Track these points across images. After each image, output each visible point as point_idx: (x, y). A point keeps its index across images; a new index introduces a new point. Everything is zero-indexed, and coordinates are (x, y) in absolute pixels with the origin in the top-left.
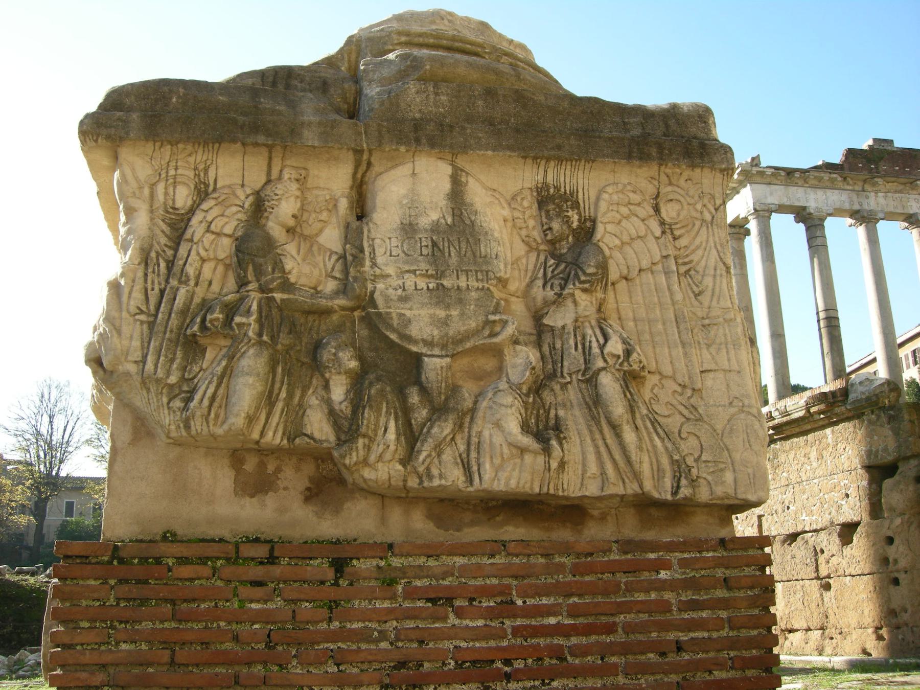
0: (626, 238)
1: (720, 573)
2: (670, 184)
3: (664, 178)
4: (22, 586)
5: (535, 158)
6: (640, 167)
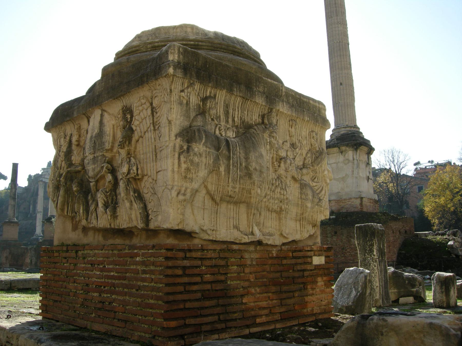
0: (140, 120)
1: (152, 259)
2: (155, 90)
3: (152, 88)
4: (433, 241)
5: (117, 98)
6: (143, 87)
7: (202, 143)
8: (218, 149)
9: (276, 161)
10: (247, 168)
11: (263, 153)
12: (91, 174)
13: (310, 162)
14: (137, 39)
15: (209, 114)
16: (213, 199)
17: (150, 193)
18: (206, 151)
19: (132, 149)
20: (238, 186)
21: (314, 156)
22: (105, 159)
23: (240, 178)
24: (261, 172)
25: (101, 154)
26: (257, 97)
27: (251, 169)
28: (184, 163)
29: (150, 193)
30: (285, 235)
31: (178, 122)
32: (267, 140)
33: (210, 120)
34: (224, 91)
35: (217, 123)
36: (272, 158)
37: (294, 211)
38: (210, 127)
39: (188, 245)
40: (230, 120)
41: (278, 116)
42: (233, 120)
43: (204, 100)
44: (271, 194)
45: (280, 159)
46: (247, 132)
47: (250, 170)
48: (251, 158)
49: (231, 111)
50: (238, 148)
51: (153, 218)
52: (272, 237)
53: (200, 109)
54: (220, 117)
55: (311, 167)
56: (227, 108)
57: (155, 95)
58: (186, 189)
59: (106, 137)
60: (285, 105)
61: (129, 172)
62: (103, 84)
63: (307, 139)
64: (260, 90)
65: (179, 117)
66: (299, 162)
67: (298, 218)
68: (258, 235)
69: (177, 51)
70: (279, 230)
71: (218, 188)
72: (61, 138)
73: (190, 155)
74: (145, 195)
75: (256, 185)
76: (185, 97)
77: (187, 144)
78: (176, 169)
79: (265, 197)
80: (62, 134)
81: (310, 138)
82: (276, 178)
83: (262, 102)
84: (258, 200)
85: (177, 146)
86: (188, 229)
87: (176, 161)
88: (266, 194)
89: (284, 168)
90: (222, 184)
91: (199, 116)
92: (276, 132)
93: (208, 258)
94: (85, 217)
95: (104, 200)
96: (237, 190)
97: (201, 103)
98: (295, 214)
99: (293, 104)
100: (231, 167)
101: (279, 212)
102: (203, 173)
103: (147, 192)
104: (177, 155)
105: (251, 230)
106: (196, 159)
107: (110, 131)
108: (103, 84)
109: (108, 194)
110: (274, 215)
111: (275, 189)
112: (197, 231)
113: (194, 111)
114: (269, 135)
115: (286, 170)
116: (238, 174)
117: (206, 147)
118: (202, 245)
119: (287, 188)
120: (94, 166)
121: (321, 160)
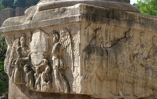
2: (72, 26)
7: (95, 54)
8: (102, 55)
9: (132, 57)
11: (125, 54)
13: (152, 54)
15: (98, 37)
16: (100, 79)
17: (70, 76)
18: (97, 57)
19: (60, 54)
20: (112, 72)
21: (155, 50)
24: (123, 64)
27: (118, 63)
28: (87, 64)
29: (70, 76)
30: (136, 95)
31: (84, 44)
32: (127, 46)
33: (98, 40)
34: (105, 24)
35: (102, 41)
36: (130, 55)
37: (141, 82)
38: (98, 45)
40: (108, 38)
41: (134, 32)
42: (110, 38)
43: (96, 31)
44: (129, 74)
45: (135, 56)
46: (116, 43)
47: (117, 64)
48: (118, 57)
49: (108, 34)
50: (112, 53)
52: (129, 96)
53: (93, 36)
55: (153, 57)
57: (72, 29)
58: (88, 76)
60: (138, 25)
61: (59, 65)
63: (151, 41)
65: (84, 41)
66: (145, 55)
67: (144, 86)
68: (122, 95)
69: (83, 8)
70: (133, 93)
72: (12, 39)
73: (90, 60)
74: (67, 77)
75: (121, 71)
76: (87, 31)
77: (88, 55)
78: (83, 67)
79: (126, 76)
81: (153, 40)
82: (131, 65)
83: (125, 26)
84: (121, 78)
85: (84, 56)
86: (88, 94)
87: (83, 63)
88: (126, 74)
89: (136, 60)
90: (104, 72)
91: (93, 40)
92: (132, 41)
94: (33, 85)
96: (111, 74)
97: (94, 33)
98: (142, 84)
99: (143, 23)
100: (108, 63)
101: (133, 83)
102: (95, 68)
103: (68, 76)
104: (84, 60)
105: (118, 93)
106: (92, 62)
110: (130, 85)
111: (131, 71)
112: (93, 95)
114: (129, 44)
115: (137, 61)
117: (97, 55)
119: (137, 71)
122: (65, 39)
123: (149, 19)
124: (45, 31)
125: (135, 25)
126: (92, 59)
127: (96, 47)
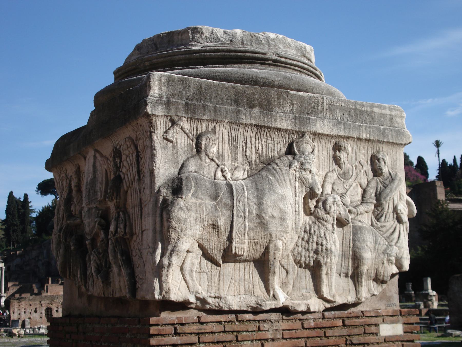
10: (259, 216)
12: (87, 229)
14: (137, 52)
15: (250, 163)
22: (99, 212)
23: (248, 231)
25: (94, 205)
26: (278, 120)
27: (266, 217)
38: (208, 170)
39: (178, 318)
47: (264, 219)
48: (265, 203)
50: (246, 193)
51: (139, 286)
54: (222, 155)
56: (234, 141)
59: (99, 184)
62: (95, 116)
64: (285, 109)
71: (217, 245)
72: (63, 180)
80: (64, 175)
87: (158, 219)
93: (207, 333)
94: (83, 283)
95: (97, 263)
107: (102, 177)
108: (95, 116)
109: (101, 256)
113: (184, 153)
116: (245, 227)
117: (197, 198)
118: (198, 317)
120: (89, 220)
121: (391, 191)
122: (129, 162)
123: (361, 111)
124: (102, 151)
125: (318, 125)
126: (181, 208)
127: (196, 178)
